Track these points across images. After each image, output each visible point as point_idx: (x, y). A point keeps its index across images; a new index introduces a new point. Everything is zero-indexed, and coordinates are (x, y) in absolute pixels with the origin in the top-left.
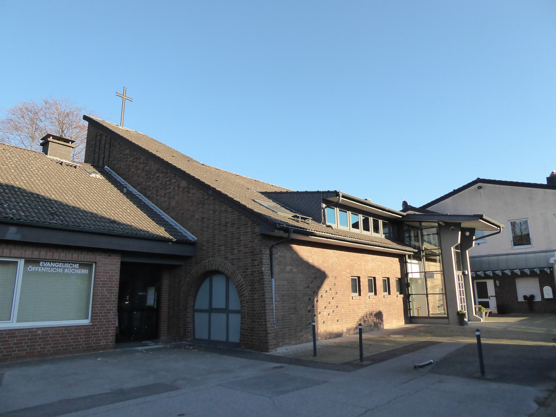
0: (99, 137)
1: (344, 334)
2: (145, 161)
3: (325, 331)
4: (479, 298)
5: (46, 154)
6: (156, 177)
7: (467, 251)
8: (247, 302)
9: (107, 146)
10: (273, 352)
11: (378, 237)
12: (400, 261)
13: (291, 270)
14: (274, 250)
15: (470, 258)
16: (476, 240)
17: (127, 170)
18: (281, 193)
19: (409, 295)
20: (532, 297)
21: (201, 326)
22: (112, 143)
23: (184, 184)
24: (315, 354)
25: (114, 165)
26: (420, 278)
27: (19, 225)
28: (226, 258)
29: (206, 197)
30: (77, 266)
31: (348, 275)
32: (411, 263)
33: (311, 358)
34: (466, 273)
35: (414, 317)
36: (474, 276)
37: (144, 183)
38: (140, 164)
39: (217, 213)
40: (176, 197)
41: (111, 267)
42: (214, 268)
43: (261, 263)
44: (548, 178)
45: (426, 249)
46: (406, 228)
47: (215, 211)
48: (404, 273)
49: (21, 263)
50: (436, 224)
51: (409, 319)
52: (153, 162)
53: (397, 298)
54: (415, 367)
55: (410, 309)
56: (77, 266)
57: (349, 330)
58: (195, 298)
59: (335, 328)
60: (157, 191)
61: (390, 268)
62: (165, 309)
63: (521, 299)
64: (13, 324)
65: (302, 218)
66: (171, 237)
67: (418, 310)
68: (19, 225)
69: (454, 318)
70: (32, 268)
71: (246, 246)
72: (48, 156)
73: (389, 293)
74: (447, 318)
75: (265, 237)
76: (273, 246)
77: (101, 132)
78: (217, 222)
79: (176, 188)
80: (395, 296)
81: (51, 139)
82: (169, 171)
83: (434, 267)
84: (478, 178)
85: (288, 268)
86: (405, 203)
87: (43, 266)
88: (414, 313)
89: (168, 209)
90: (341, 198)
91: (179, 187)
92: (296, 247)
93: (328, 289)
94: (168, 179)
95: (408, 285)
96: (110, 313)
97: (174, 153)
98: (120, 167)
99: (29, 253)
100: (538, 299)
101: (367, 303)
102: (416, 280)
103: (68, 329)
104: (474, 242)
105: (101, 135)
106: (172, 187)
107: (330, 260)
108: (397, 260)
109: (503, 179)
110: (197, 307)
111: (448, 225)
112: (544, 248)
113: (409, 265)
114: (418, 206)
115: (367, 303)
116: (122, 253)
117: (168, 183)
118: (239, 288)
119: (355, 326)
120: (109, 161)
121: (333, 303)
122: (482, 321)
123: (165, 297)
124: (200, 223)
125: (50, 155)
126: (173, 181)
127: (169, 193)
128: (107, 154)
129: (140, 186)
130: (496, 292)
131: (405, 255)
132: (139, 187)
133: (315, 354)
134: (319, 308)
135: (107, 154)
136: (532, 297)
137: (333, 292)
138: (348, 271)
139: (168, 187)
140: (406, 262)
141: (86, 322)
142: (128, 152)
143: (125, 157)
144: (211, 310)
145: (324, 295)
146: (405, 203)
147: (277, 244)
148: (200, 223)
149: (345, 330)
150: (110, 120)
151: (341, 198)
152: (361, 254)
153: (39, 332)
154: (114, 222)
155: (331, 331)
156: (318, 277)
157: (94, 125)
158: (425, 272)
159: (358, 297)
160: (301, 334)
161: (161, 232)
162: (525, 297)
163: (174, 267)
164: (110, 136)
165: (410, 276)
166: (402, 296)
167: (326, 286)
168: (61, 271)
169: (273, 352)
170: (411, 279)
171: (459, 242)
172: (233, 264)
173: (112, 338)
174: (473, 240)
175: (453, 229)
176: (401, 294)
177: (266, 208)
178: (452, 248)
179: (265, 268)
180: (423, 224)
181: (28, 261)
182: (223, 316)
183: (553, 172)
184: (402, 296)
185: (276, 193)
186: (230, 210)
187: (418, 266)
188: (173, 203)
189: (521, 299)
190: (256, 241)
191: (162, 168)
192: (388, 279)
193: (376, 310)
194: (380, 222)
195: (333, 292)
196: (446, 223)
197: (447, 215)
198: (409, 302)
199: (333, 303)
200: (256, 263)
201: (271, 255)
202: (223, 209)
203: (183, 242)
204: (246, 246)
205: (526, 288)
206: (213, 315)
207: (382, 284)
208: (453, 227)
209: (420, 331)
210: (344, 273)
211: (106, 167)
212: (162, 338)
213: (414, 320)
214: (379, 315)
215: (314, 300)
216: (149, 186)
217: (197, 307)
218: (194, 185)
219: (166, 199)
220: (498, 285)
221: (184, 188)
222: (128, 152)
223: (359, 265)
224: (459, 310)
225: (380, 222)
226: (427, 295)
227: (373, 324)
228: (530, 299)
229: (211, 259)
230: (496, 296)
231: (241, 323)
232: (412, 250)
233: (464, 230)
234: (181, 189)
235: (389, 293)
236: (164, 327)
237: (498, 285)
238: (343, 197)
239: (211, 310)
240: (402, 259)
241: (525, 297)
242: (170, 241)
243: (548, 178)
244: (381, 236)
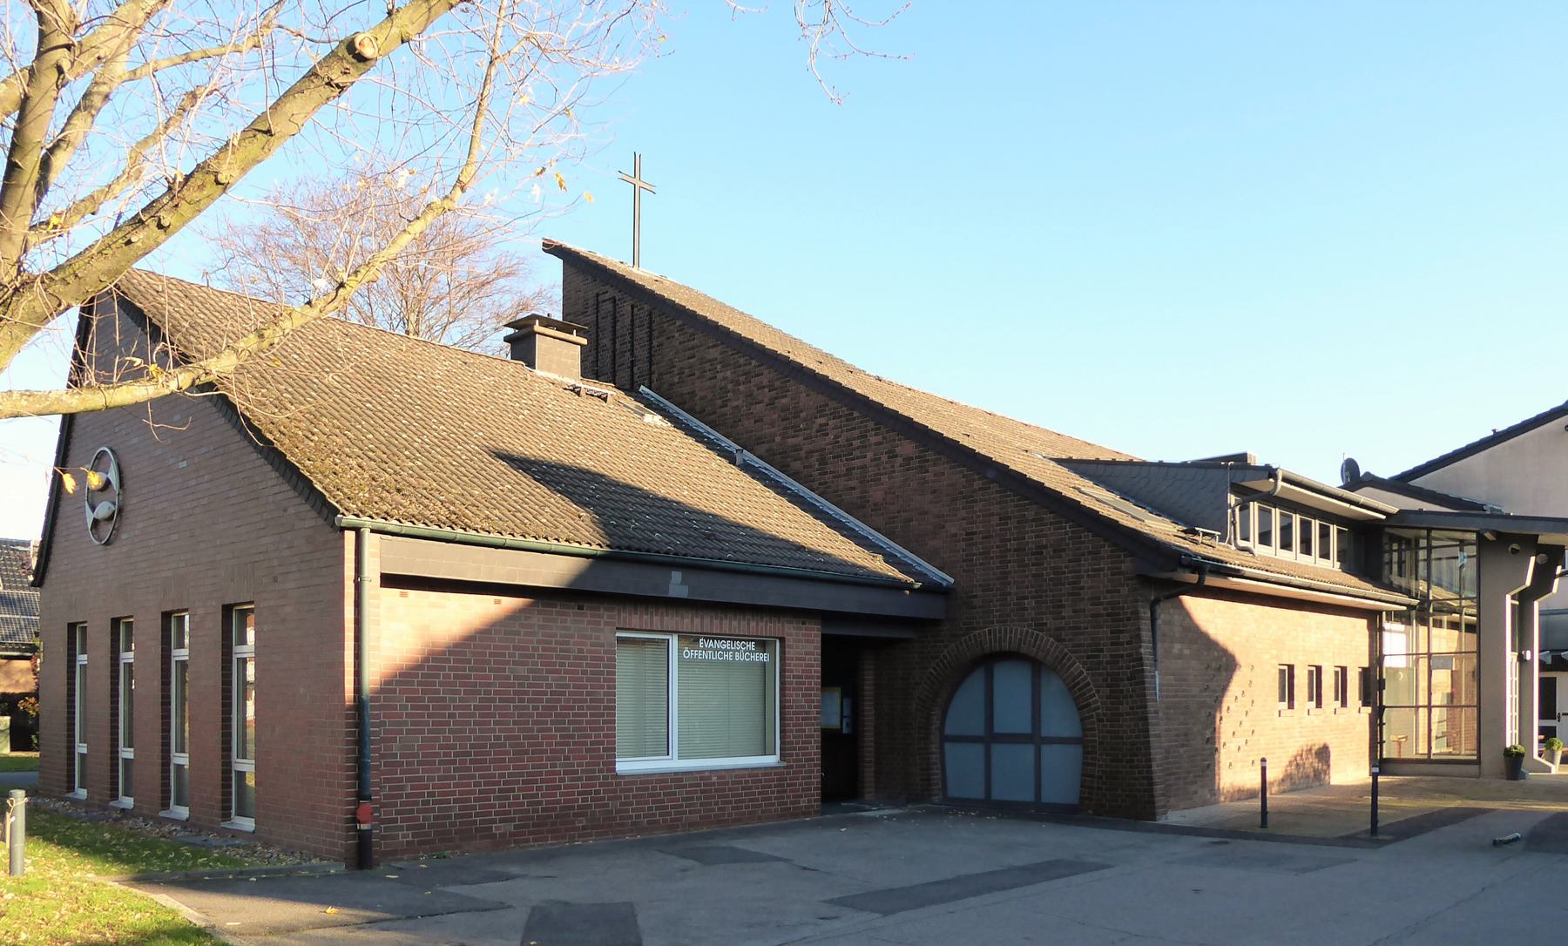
0: (607, 307)
2: (777, 384)
5: (531, 364)
6: (815, 427)
8: (1100, 720)
9: (641, 334)
10: (1162, 821)
11: (1322, 569)
13: (1181, 650)
14: (1159, 610)
15: (1540, 614)
17: (719, 402)
18: (1114, 463)
21: (962, 768)
22: (655, 326)
23: (907, 448)
24: (1264, 823)
25: (672, 385)
26: (1408, 668)
28: (1040, 626)
29: (977, 484)
30: (751, 646)
33: (1259, 830)
34: (1528, 657)
35: (1389, 760)
36: (1549, 661)
37: (778, 439)
38: (761, 388)
39: (1012, 524)
40: (884, 478)
41: (806, 644)
42: (1006, 647)
43: (1138, 638)
45: (1435, 600)
46: (1385, 540)
47: (1004, 519)
48: (1377, 657)
49: (674, 641)
50: (1473, 536)
51: (1380, 764)
52: (802, 388)
53: (1358, 715)
54: (1495, 843)
56: (751, 646)
58: (944, 713)
60: (823, 461)
61: (1338, 643)
62: (869, 738)
64: (672, 763)
65: (1205, 534)
66: (901, 576)
69: (1492, 760)
70: (690, 653)
71: (1095, 601)
72: (537, 372)
73: (1291, 706)
74: (1478, 762)
75: (1145, 580)
76: (1156, 602)
77: (612, 292)
78: (1012, 545)
79: (884, 458)
81: (537, 328)
82: (856, 414)
83: (1445, 640)
85: (1177, 647)
86: (1350, 467)
87: (705, 649)
89: (863, 507)
90: (1280, 484)
91: (892, 455)
92: (1188, 600)
93: (1239, 694)
94: (856, 433)
97: (826, 358)
98: (693, 393)
99: (689, 621)
101: (1304, 726)
102: (1396, 671)
103: (721, 773)
104: (1557, 581)
105: (614, 300)
106: (870, 455)
108: (1363, 622)
110: (948, 731)
111: (1503, 539)
113: (1386, 635)
114: (1386, 472)
115: (1304, 726)
116: (825, 617)
117: (856, 443)
118: (1077, 694)
120: (651, 373)
121: (1247, 725)
123: (869, 709)
124: (963, 544)
125: (541, 369)
126: (873, 439)
127: (864, 467)
128: (641, 353)
129: (765, 447)
131: (1380, 612)
132: (763, 449)
133: (1264, 823)
135: (641, 353)
137: (1247, 699)
138: (1274, 652)
139: (857, 453)
140: (1381, 629)
141: (772, 760)
142: (714, 353)
143: (707, 366)
144: (991, 738)
145: (1232, 707)
146: (1350, 467)
147: (1167, 598)
148: (963, 544)
150: (611, 252)
151: (1280, 484)
153: (714, 779)
154: (801, 548)
157: (577, 266)
159: (1314, 710)
160: (1193, 788)
161: (878, 565)
163: (891, 643)
164: (646, 307)
166: (1369, 710)
167: (1235, 688)
168: (728, 656)
169: (1162, 821)
171: (1528, 583)
172: (1059, 639)
173: (816, 794)
174: (1555, 577)
175: (1514, 551)
176: (1365, 704)
178: (1508, 597)
179: (1145, 650)
180: (1434, 533)
181: (690, 638)
182: (1028, 752)
184: (1369, 710)
185: (1097, 462)
186: (1049, 517)
188: (877, 494)
190: (1125, 590)
191: (832, 404)
192: (1291, 667)
193: (1318, 743)
194: (1334, 529)
195: (1247, 699)
196: (1498, 534)
197: (1508, 516)
199: (1247, 725)
200: (1124, 638)
201: (1153, 620)
202: (1030, 514)
203: (931, 589)
204: (1095, 601)
206: (998, 750)
207: (1333, 681)
208: (1515, 546)
209: (1424, 789)
211: (642, 388)
212: (868, 797)
214: (1323, 753)
216: (797, 448)
217: (948, 731)
219: (853, 483)
221: (908, 460)
222: (714, 353)
225: (1334, 529)
226: (1430, 707)
229: (997, 626)
231: (1084, 764)
232: (1406, 599)
233: (1540, 549)
234: (899, 460)
235: (1291, 706)
236: (869, 773)
238: (1285, 480)
239: (991, 738)
240: (1373, 618)
242: (909, 586)
244: (1332, 565)
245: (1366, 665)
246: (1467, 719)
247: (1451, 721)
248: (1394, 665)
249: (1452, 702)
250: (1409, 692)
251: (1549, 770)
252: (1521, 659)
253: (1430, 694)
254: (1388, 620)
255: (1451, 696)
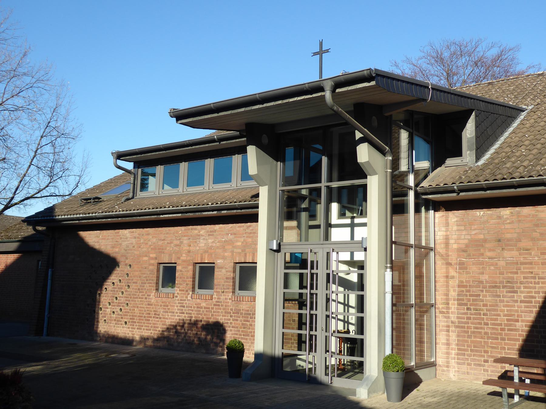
1: (134, 343)
3: (105, 332)
4: (229, 180)
31: (152, 262)
57: (144, 340)
59: (122, 331)
92: (84, 234)
107: (124, 244)
119: (156, 337)
134: (101, 304)
138: (153, 255)
149: (137, 338)
152: (183, 228)
155: (115, 334)
156: (106, 264)
167: (114, 277)
177: (21, 182)
210: (145, 259)
215: (96, 293)
218: (173, 338)
223: (176, 245)
227: (196, 341)
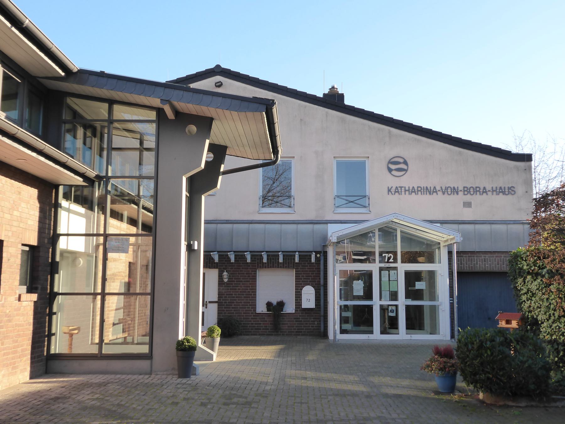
7: (203, 197)
12: (41, 199)
15: (205, 223)
16: (225, 173)
19: (53, 295)
20: (281, 304)
26: (86, 255)
27: (521, 407)
32: (68, 210)
44: (324, 94)
48: (49, 233)
51: (44, 362)
55: (50, 335)
63: (261, 308)
67: (71, 335)
68: (521, 407)
69: (165, 355)
74: (148, 357)
80: (13, 299)
84: (218, 66)
88: (58, 346)
95: (54, 268)
96: (240, 284)
100: (290, 308)
102: (73, 255)
104: (220, 177)
109: (262, 77)
112: (311, 216)
113: (63, 215)
122: (215, 359)
130: (220, 295)
136: (281, 304)
140: (57, 206)
158: (106, 236)
162: (269, 305)
165: (63, 244)
166: (34, 297)
170: (63, 252)
176: (30, 290)
183: (333, 87)
184: (34, 297)
187: (84, 220)
189: (261, 308)
196: (177, 113)
198: (51, 314)
205: (274, 288)
213: (57, 365)
220: (226, 280)
224: (181, 337)
226: (104, 294)
228: (276, 308)
230: (220, 303)
237: (226, 280)
240: (47, 190)
241: (269, 305)
243: (324, 94)
245: (34, 241)
246: (142, 305)
247: (127, 309)
248: (71, 248)
249: (129, 291)
250: (88, 278)
251: (210, 357)
252: (190, 248)
253: (104, 279)
254: (67, 196)
255: (128, 285)
